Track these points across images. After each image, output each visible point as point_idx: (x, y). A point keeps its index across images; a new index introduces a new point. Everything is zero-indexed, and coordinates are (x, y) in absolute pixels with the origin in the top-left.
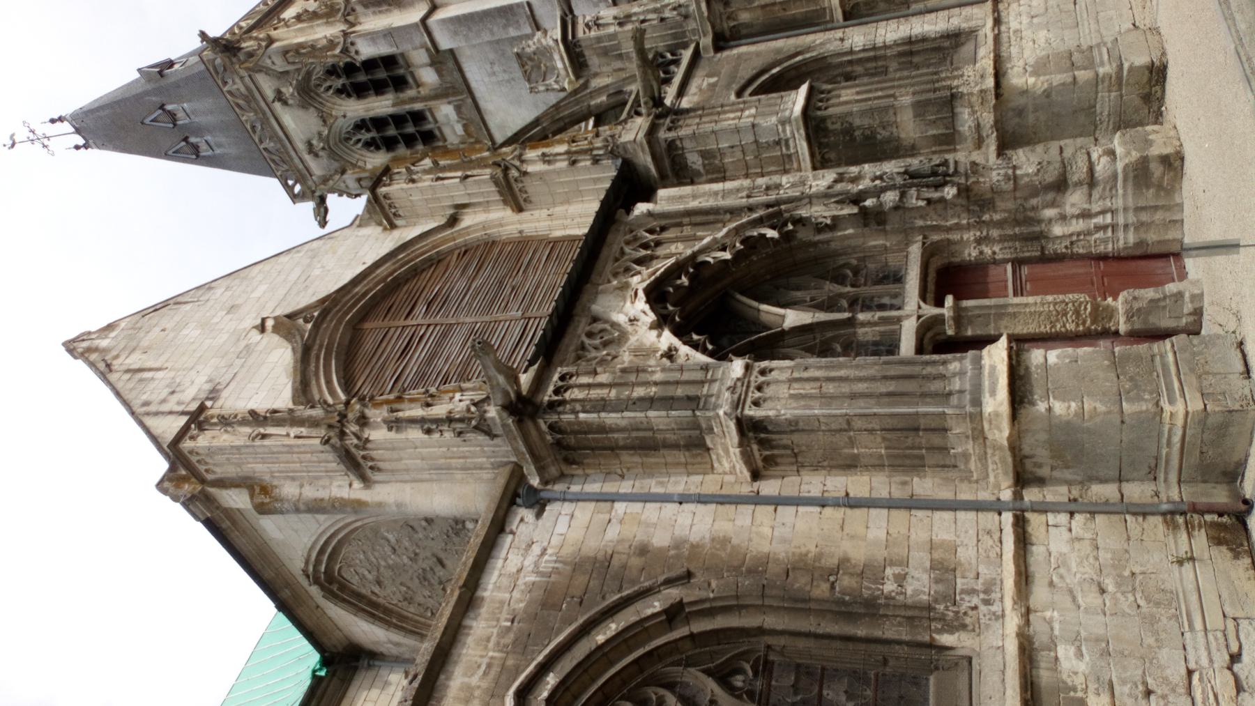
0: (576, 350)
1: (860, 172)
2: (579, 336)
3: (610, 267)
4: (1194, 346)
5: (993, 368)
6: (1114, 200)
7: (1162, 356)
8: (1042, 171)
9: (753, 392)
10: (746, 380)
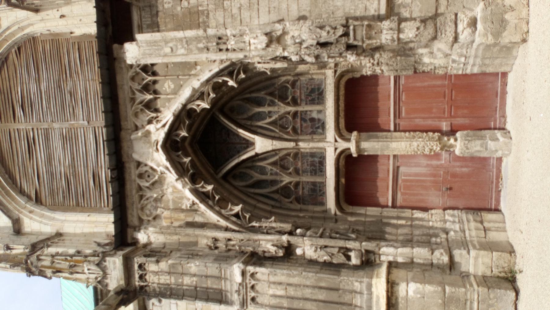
0: (138, 192)
1: (284, 29)
2: (135, 181)
3: (130, 113)
4: (490, 299)
5: (378, 297)
6: (468, 50)
7: (471, 303)
8: (419, 36)
9: (250, 292)
10: (244, 284)
